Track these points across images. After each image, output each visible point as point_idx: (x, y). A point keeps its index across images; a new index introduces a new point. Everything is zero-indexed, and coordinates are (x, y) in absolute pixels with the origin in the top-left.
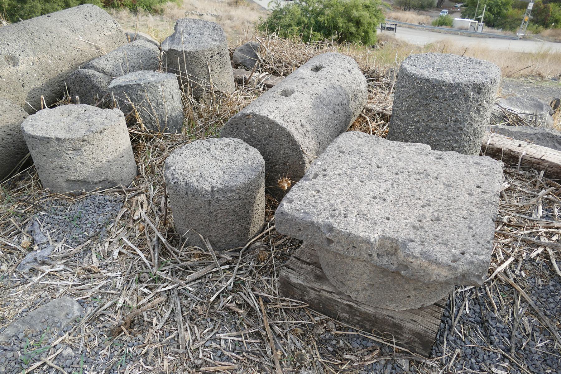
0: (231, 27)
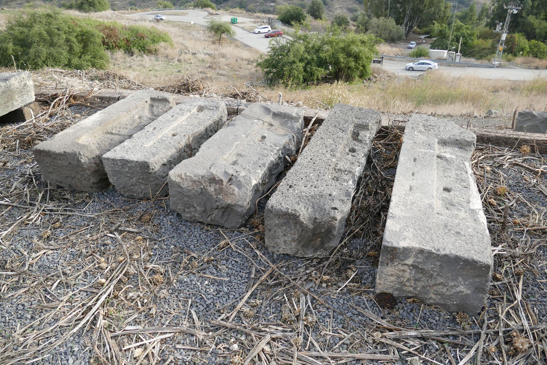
0: (227, 65)
